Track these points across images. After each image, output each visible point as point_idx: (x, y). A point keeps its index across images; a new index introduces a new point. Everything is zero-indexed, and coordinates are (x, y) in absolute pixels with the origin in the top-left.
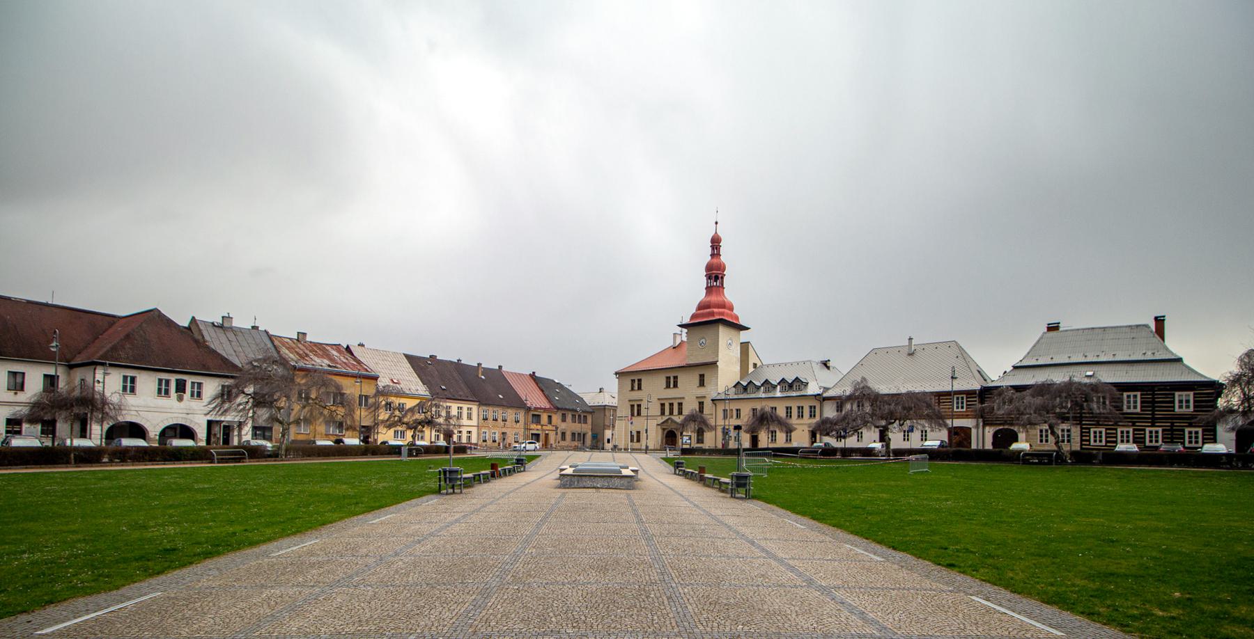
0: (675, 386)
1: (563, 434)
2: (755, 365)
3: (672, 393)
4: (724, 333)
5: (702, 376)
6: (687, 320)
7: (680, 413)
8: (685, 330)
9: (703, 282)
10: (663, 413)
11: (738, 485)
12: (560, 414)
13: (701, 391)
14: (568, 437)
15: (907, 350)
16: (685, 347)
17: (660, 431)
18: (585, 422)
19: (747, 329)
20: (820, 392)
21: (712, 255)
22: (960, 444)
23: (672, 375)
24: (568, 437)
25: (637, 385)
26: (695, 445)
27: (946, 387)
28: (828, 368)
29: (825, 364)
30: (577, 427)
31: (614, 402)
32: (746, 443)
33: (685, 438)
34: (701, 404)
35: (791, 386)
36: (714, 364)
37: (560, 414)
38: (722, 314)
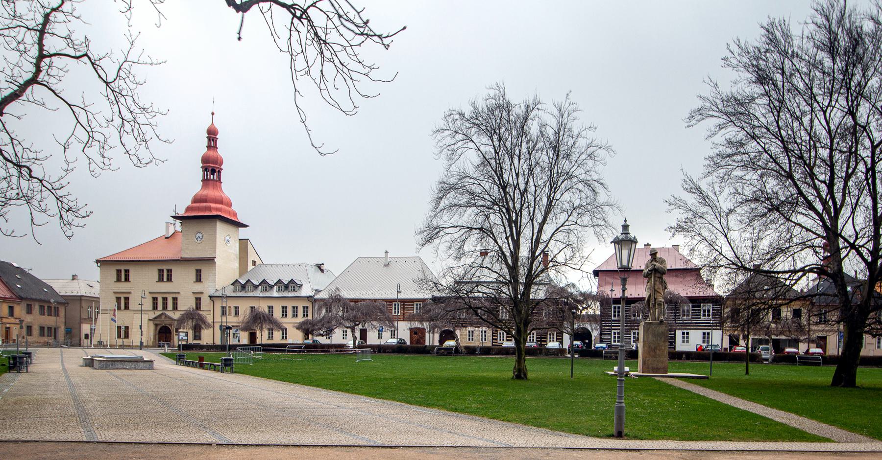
0: (169, 279)
1: (29, 329)
2: (254, 263)
3: (165, 287)
4: (221, 230)
5: (199, 273)
6: (182, 212)
7: (175, 308)
8: (178, 222)
9: (198, 174)
10: (155, 307)
11: (226, 365)
12: (24, 305)
13: (198, 287)
14: (36, 331)
15: (383, 262)
16: (180, 237)
17: (152, 327)
18: (57, 315)
19: (246, 226)
20: (312, 294)
21: (209, 147)
22: (418, 342)
23: (165, 268)
24: (36, 331)
25: (123, 276)
26: (191, 341)
27: (393, 296)
28: (322, 271)
29: (320, 267)
30: (49, 321)
31: (95, 292)
32: (244, 338)
33: (182, 335)
34: (198, 300)
35: (286, 287)
36: (211, 261)
37: (24, 305)
38: (217, 209)
